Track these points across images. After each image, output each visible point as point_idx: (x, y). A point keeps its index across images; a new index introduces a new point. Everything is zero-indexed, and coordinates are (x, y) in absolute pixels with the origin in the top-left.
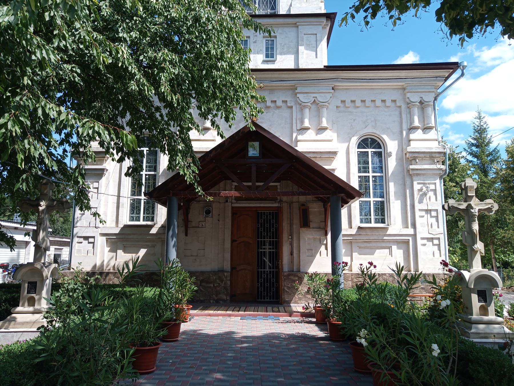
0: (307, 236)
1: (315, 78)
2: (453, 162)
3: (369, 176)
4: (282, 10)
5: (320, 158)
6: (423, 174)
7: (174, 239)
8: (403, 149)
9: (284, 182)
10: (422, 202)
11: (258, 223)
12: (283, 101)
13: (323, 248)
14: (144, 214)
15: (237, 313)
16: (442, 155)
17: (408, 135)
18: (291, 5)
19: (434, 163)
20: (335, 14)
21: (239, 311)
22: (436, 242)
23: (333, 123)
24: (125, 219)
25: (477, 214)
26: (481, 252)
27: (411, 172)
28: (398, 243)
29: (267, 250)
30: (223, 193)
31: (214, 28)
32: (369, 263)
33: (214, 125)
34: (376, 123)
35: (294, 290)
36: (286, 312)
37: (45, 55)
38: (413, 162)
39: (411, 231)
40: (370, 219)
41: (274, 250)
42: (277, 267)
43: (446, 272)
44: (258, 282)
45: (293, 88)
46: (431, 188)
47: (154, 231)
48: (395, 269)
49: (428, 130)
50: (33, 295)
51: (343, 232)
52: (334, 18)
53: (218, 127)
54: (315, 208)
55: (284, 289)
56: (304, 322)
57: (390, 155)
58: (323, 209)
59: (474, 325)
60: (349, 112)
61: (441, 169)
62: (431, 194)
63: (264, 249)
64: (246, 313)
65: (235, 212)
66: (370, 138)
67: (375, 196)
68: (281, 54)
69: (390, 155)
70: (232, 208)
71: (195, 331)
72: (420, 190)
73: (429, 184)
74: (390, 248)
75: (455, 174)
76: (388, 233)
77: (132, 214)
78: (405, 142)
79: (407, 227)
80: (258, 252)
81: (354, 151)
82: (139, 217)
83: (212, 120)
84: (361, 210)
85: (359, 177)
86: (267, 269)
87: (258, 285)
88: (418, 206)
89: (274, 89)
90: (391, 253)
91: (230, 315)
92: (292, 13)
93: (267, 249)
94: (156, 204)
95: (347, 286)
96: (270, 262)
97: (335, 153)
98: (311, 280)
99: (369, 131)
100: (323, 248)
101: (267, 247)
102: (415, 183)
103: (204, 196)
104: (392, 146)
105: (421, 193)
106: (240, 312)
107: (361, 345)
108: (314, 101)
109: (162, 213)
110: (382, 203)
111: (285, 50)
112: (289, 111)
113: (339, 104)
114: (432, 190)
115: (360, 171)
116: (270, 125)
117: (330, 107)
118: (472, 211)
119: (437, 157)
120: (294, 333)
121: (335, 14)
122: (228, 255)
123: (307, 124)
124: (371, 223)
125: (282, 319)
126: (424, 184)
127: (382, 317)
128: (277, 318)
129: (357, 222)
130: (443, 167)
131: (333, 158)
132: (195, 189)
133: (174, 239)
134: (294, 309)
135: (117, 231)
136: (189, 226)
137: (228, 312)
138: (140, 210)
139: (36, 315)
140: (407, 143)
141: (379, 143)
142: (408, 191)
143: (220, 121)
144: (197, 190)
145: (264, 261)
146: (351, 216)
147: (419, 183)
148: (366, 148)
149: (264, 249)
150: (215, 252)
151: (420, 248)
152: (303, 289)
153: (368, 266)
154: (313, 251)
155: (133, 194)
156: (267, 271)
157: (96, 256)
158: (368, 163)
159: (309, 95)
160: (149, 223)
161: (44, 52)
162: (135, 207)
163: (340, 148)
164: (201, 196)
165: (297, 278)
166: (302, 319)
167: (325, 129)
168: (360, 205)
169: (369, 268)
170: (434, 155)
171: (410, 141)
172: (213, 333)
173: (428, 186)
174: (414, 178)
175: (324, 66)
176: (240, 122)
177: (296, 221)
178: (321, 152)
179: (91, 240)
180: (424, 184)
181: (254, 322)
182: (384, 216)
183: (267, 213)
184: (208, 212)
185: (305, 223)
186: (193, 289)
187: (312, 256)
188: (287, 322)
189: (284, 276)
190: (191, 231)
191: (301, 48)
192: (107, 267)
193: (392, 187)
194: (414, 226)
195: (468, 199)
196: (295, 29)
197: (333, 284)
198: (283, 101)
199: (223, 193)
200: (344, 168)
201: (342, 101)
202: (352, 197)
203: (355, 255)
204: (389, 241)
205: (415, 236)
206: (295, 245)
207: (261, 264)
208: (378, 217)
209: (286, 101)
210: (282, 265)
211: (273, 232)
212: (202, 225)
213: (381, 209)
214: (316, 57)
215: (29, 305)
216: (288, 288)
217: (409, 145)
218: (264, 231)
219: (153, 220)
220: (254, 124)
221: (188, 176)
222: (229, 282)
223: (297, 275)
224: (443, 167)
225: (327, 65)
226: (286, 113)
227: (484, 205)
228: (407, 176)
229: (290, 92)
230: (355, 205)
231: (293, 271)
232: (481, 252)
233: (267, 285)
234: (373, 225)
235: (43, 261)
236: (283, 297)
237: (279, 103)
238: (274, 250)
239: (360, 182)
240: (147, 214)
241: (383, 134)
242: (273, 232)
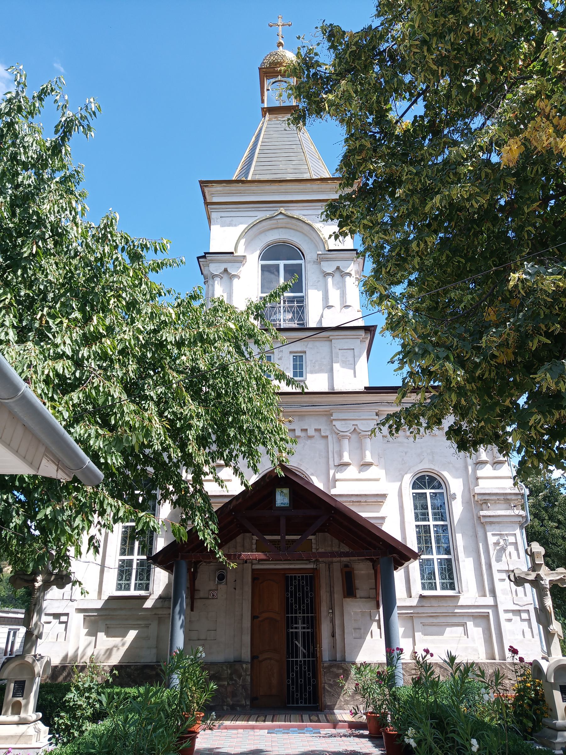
0: (353, 609)
1: (355, 402)
2: (551, 493)
3: (429, 526)
4: (312, 323)
5: (366, 502)
6: (499, 523)
7: (182, 617)
8: (469, 489)
9: (320, 534)
10: (501, 561)
11: (287, 591)
12: (315, 430)
13: (374, 626)
14: (136, 580)
15: (262, 723)
16: (520, 497)
17: (474, 471)
18: (322, 316)
19: (511, 508)
20: (375, 327)
21: (264, 721)
22: (525, 616)
23: (380, 457)
24: (111, 589)
25: (548, 586)
26: (558, 635)
27: (483, 520)
28: (475, 617)
29: (300, 631)
30: (245, 555)
31: (243, 378)
32: (425, 650)
33: (237, 473)
34: (433, 457)
35: (338, 689)
36: (328, 721)
37: (114, 461)
38: (484, 506)
39: (489, 601)
40: (435, 583)
41: (309, 630)
42: (314, 655)
43: (515, 661)
44: (288, 677)
45: (328, 413)
46: (510, 541)
47: (149, 604)
48: (447, 660)
49: (499, 465)
50: (18, 699)
51: (398, 603)
52: (375, 331)
53: (241, 475)
54: (363, 570)
55: (324, 688)
56: (354, 736)
57: (454, 497)
58: (373, 572)
59: (559, 733)
60: (399, 442)
61: (521, 515)
62: (511, 549)
63: (296, 628)
64: (275, 723)
65: (258, 577)
66: (428, 476)
67: (439, 553)
68: (312, 372)
69: (454, 497)
70: (253, 570)
71: (211, 750)
72: (497, 544)
73: (507, 535)
74: (464, 625)
75: (556, 509)
76: (460, 603)
77: (120, 580)
78: (471, 480)
79: (485, 596)
80: (288, 633)
81: (408, 493)
82: (129, 585)
83: (234, 467)
84: (422, 571)
85: (417, 526)
86: (301, 658)
87: (289, 682)
88: (496, 566)
89: (305, 415)
90: (466, 633)
91: (253, 728)
92: (324, 325)
93: (300, 628)
94: (153, 566)
95: (404, 682)
96: (304, 648)
97: (384, 496)
98: (359, 674)
99: (425, 466)
100: (374, 626)
101: (300, 625)
102: (489, 534)
103: (226, 562)
104: (456, 485)
105: (498, 548)
106: (267, 723)
107: (409, 745)
109: (161, 579)
110: (449, 560)
111: (317, 367)
112: (323, 441)
114: (511, 544)
115: (417, 519)
116: (301, 460)
118: (542, 582)
119: (514, 500)
120: (341, 750)
121: (375, 327)
122: (247, 639)
123: (346, 458)
124: (436, 589)
125: (323, 732)
126: (500, 535)
127: (441, 720)
128: (316, 731)
129: (417, 589)
130: (522, 513)
131: (382, 502)
132: (216, 554)
133: (182, 617)
134: (339, 718)
135: (99, 605)
136: (196, 597)
137: (251, 723)
138: (130, 575)
139: (21, 726)
140: (474, 481)
142: (481, 545)
143: (242, 463)
144: (218, 556)
145: (296, 645)
146: (407, 583)
147: (493, 535)
150: (229, 632)
151: (505, 626)
152: (349, 687)
153: (424, 654)
154: (362, 631)
155: (123, 553)
156: (301, 661)
157: (69, 641)
158: (427, 508)
159: (348, 422)
160: (143, 593)
161: (114, 458)
162: (124, 571)
163: (389, 488)
164: (222, 562)
165: (341, 671)
166: (350, 732)
167: (369, 465)
168: (421, 565)
169: (425, 656)
170: (509, 497)
171: (477, 479)
172: (235, 752)
173: (506, 538)
174: (488, 528)
175: (366, 388)
176: (265, 465)
177: (338, 588)
178: (366, 495)
179: (64, 619)
180: (500, 535)
181: (286, 736)
182: (453, 579)
183: (299, 577)
184: (221, 578)
185: (350, 591)
186: (212, 688)
187: (360, 638)
188: (331, 736)
189: (324, 668)
190: (198, 603)
191: (336, 366)
192: (81, 658)
193: (460, 541)
194: (493, 593)
195: (536, 568)
196: (327, 343)
197: (387, 678)
198: (315, 430)
199: (245, 555)
200: (397, 521)
202: (408, 559)
203: (418, 635)
204: (462, 615)
205: (495, 607)
206: (337, 622)
207: (292, 651)
208: (445, 581)
209: (320, 430)
210: (321, 651)
212: (213, 595)
213: (449, 570)
214: (355, 376)
215: (13, 713)
216: (331, 686)
217: (477, 485)
218: (296, 603)
219: (147, 589)
220: (284, 468)
221: (208, 541)
222: (248, 678)
223: (342, 666)
224: (522, 513)
225: (368, 385)
226: (319, 444)
227: (555, 575)
228: (480, 525)
229: (324, 419)
230: (414, 566)
231: (336, 660)
232: (558, 635)
233: (301, 681)
234: (439, 592)
235: (33, 653)
236: (323, 699)
237: (311, 432)
238: (309, 630)
239: (418, 533)
240: (140, 580)
241: (444, 470)
242: (307, 604)
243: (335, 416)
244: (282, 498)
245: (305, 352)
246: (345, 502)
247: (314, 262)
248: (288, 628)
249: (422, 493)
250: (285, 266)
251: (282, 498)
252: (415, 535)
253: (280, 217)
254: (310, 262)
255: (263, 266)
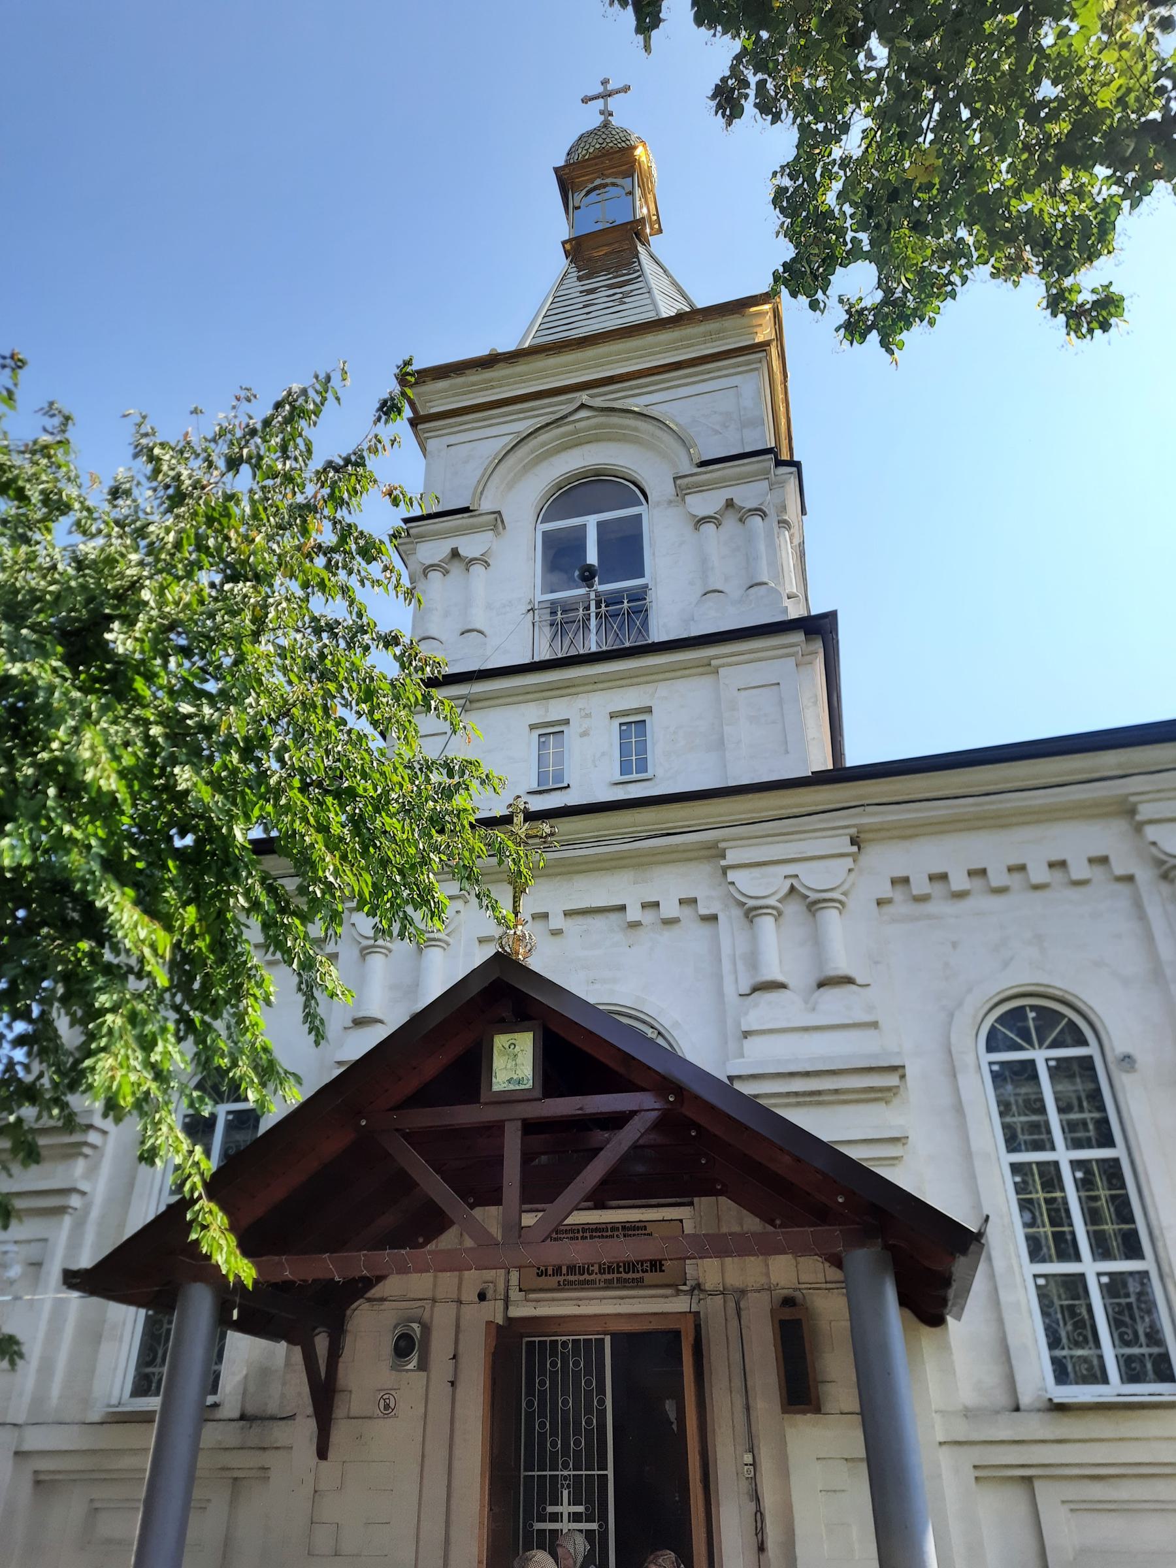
12: (681, 902)
60: (930, 917)
63: (555, 1517)
66: (1033, 1008)
67: (1102, 1250)
81: (976, 1069)
85: (1016, 1168)
108: (792, 889)
112: (705, 929)
113: (886, 891)
115: (1012, 1144)
117: (851, 903)
124: (1105, 1381)
141: (1072, 1024)
148: (1020, 1048)
149: (555, 1517)
158: (1042, 1110)
190: (340, 1434)
196: (707, 681)
198: (681, 902)
201: (894, 882)
208: (1135, 1351)
211: (577, 1432)
226: (693, 936)
237: (670, 909)
243: (732, 857)
244: (514, 1062)
245: (649, 710)
246: (775, 1105)
247: (670, 502)
248: (529, 1517)
249: (1023, 1063)
250: (600, 525)
251: (514, 1062)
252: (1013, 1198)
253: (583, 414)
254: (658, 504)
255: (549, 540)
